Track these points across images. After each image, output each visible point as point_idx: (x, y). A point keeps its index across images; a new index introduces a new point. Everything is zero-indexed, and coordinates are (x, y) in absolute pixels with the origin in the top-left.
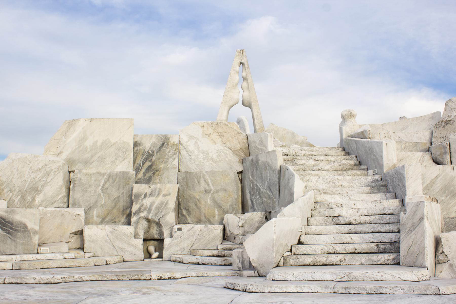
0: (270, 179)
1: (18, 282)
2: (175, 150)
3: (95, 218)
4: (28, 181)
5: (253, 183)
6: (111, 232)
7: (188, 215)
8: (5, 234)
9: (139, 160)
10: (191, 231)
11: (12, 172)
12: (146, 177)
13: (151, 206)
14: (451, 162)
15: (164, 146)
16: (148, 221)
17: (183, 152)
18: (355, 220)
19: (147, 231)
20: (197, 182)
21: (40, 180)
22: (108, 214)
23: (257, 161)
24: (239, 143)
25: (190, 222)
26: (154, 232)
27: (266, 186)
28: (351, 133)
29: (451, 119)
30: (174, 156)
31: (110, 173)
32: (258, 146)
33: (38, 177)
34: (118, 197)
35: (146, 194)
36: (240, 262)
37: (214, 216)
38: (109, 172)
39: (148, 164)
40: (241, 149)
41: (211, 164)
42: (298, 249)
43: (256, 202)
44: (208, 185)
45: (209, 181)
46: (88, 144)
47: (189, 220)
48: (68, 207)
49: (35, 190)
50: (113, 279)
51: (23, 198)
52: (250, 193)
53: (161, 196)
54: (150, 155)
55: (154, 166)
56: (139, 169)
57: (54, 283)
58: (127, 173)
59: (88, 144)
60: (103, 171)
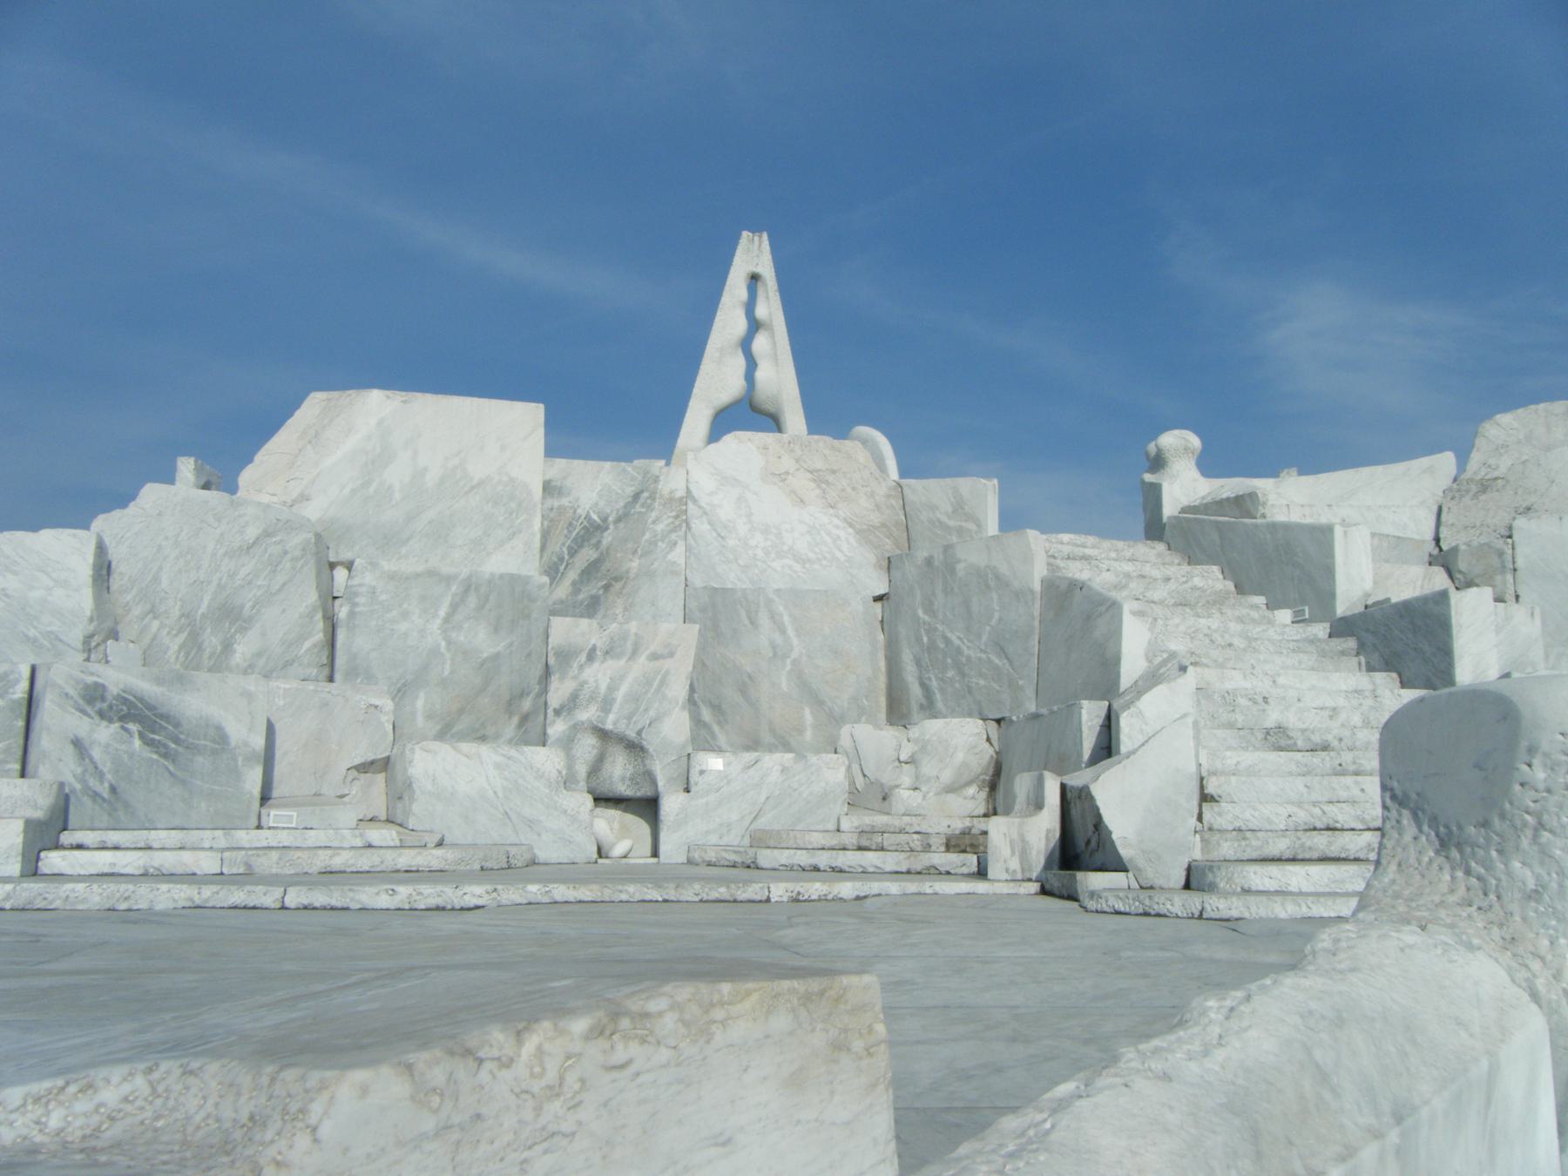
0: (1000, 619)
1: (334, 903)
2: (677, 517)
3: (420, 721)
4: (209, 583)
5: (931, 630)
6: (498, 766)
7: (719, 723)
8: (155, 756)
9: (559, 545)
10: (752, 772)
11: (160, 548)
12: (581, 597)
13: (612, 688)
14: (1517, 597)
15: (642, 500)
16: (603, 735)
17: (700, 526)
18: (1341, 740)
19: (595, 769)
20: (747, 622)
21: (250, 583)
22: (461, 711)
23: (950, 567)
24: (878, 507)
25: (725, 746)
26: (619, 774)
27: (984, 638)
28: (1185, 501)
29: (1496, 474)
30: (673, 536)
31: (470, 577)
32: (944, 519)
33: (243, 572)
34: (497, 656)
35: (594, 649)
36: (1013, 853)
37: (801, 731)
38: (465, 572)
39: (588, 554)
40: (883, 525)
41: (790, 567)
42: (1220, 814)
43: (942, 690)
44: (783, 632)
45: (786, 619)
46: (396, 475)
47: (722, 739)
48: (331, 679)
49: (231, 616)
50: (648, 897)
51: (194, 642)
52: (918, 662)
53: (642, 659)
54: (592, 530)
55: (607, 565)
56: (557, 571)
57: (462, 909)
58: (526, 580)
59: (396, 475)
60: (446, 570)
